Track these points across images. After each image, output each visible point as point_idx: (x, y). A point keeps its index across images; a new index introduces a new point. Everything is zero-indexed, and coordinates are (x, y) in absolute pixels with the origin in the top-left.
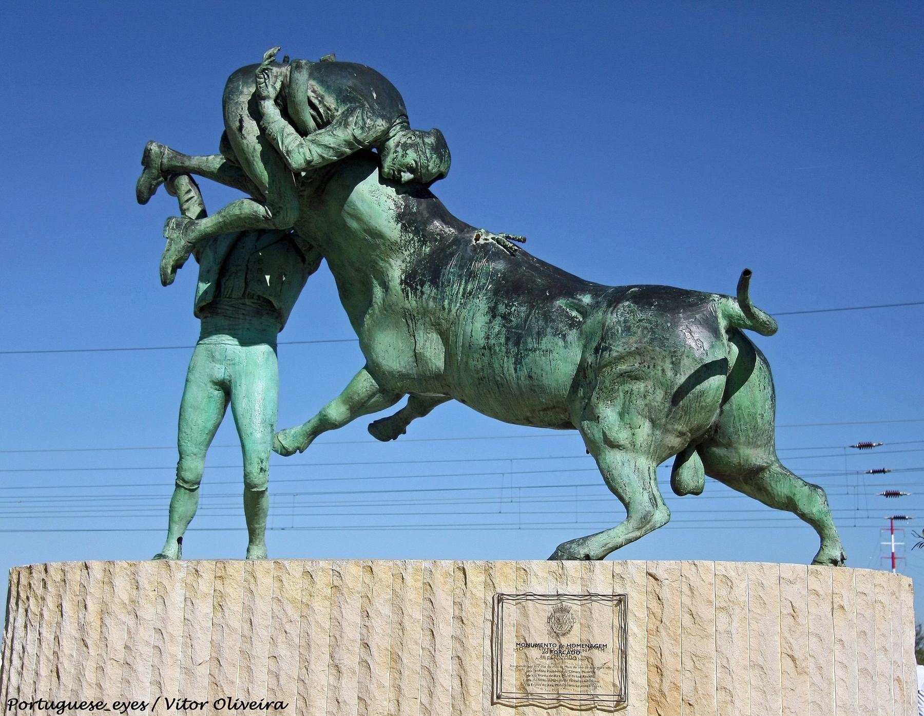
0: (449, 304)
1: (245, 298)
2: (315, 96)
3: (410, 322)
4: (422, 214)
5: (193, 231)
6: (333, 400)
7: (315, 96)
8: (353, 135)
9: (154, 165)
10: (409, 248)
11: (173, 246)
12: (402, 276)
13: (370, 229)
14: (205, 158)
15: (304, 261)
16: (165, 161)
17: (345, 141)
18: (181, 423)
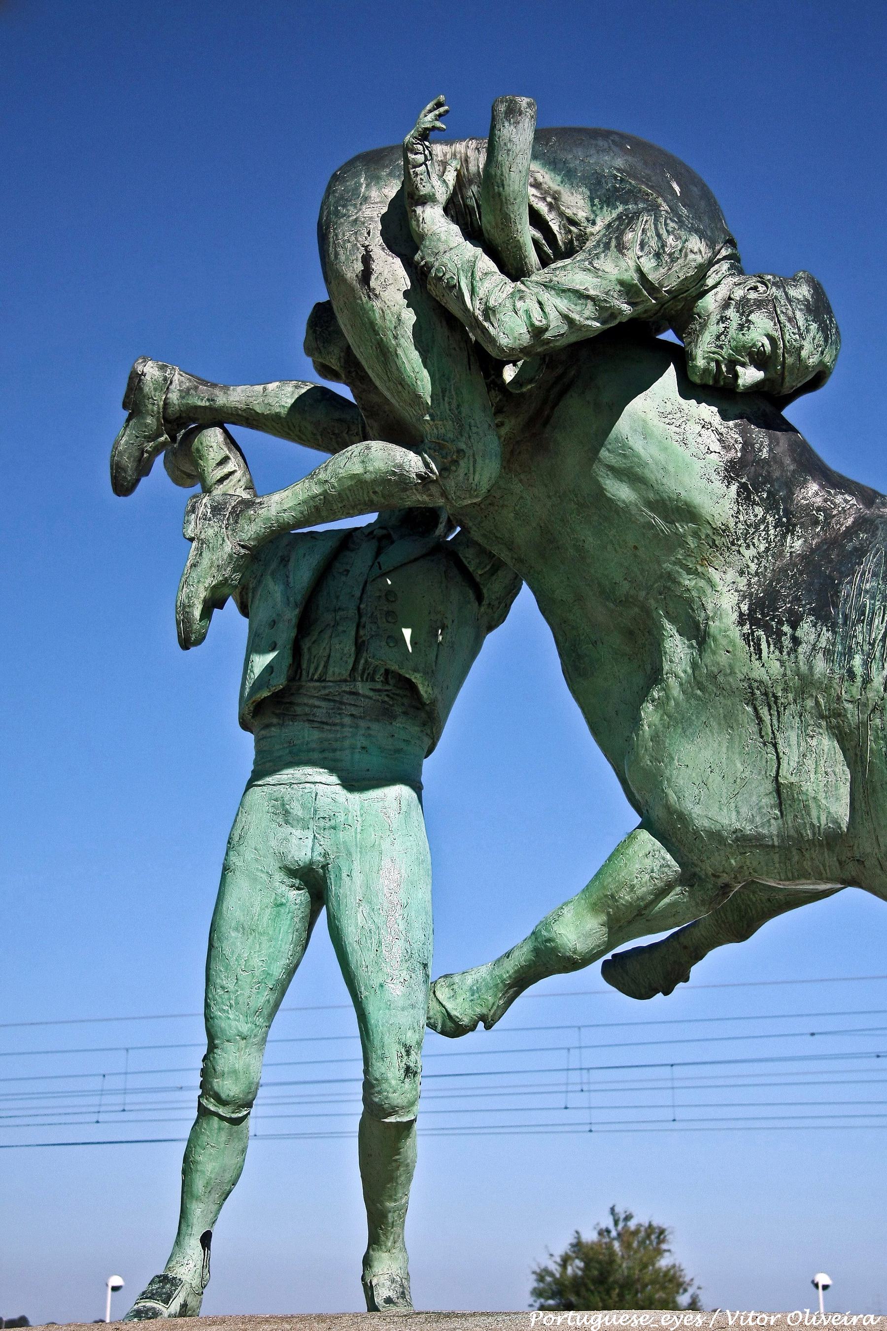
0: (866, 664)
1: (355, 680)
2: (538, 195)
3: (764, 712)
4: (781, 464)
5: (251, 521)
6: (566, 904)
7: (538, 195)
8: (639, 270)
9: (150, 406)
10: (756, 541)
11: (206, 555)
12: (742, 606)
13: (663, 500)
14: (259, 388)
15: (479, 598)
16: (174, 397)
17: (621, 283)
18: (213, 966)
